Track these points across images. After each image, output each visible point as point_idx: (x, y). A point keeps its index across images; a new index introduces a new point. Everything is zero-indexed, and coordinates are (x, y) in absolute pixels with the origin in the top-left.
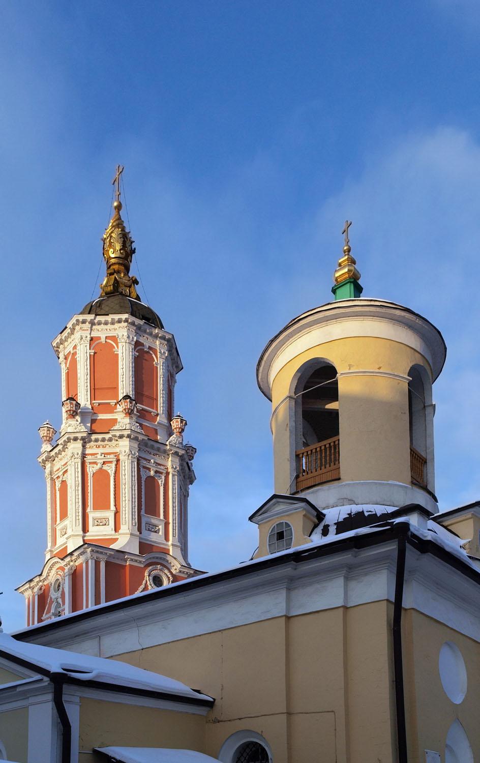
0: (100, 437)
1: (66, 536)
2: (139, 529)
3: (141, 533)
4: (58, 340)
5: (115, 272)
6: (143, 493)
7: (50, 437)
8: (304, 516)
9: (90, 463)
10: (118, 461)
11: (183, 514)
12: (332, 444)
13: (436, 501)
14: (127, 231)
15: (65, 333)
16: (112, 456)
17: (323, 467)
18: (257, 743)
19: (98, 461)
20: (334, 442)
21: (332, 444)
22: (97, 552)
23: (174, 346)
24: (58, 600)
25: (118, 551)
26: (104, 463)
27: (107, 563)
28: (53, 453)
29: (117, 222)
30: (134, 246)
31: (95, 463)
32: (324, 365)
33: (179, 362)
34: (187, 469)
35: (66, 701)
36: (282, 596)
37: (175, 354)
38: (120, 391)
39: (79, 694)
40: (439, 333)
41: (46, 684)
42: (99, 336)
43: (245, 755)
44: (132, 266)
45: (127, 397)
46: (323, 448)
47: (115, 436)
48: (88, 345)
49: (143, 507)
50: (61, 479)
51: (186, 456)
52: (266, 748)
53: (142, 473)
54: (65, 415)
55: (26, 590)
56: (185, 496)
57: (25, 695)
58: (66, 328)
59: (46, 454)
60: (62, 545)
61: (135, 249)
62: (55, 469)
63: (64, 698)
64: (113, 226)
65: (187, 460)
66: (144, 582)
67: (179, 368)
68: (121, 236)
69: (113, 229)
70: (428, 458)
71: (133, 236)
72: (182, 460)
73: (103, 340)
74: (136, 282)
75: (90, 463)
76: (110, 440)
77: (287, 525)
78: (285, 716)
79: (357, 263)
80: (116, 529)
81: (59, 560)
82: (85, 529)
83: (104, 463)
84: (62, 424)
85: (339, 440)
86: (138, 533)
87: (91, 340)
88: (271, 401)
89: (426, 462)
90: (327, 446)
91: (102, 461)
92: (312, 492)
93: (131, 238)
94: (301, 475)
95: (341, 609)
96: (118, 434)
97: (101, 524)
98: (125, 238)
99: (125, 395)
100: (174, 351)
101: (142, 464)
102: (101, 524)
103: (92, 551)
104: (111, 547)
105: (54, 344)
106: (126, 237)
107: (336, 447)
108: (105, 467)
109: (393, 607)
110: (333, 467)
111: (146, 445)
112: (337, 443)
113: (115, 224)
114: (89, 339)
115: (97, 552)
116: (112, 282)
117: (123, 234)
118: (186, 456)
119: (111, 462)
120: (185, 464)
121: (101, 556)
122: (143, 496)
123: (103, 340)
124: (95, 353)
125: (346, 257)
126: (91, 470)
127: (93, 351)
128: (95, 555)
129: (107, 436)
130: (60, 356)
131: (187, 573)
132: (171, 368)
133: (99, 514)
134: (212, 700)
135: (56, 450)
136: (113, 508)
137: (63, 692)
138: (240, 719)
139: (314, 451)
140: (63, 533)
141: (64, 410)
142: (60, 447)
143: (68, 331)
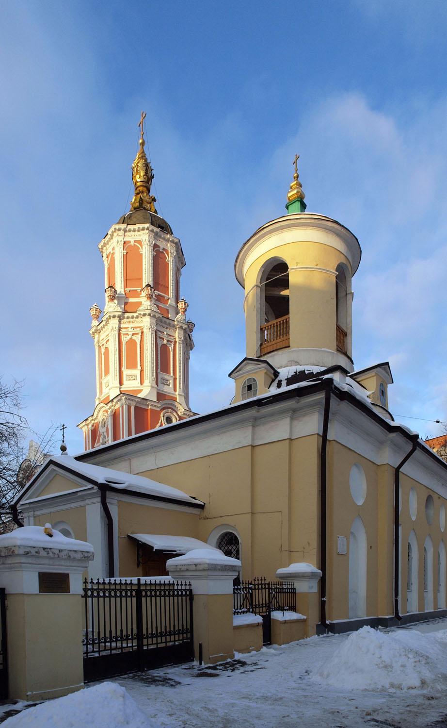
0: (130, 315)
1: (109, 388)
3: (158, 386)
4: (102, 244)
7: (97, 316)
9: (124, 334)
10: (142, 333)
12: (285, 321)
13: (353, 364)
14: (148, 161)
16: (138, 329)
17: (278, 338)
18: (232, 533)
19: (129, 333)
21: (285, 321)
23: (180, 248)
26: (133, 334)
27: (136, 408)
28: (99, 327)
30: (153, 172)
32: (279, 263)
39: (116, 498)
41: (96, 491)
42: (129, 240)
43: (224, 540)
44: (152, 188)
45: (148, 285)
46: (279, 323)
47: (140, 314)
48: (122, 247)
49: (159, 367)
50: (104, 346)
51: (188, 330)
52: (236, 534)
54: (107, 299)
56: (187, 359)
57: (83, 498)
58: (108, 234)
61: (154, 175)
63: (108, 501)
65: (188, 332)
66: (160, 421)
68: (144, 165)
71: (152, 165)
72: (185, 332)
73: (132, 243)
74: (154, 200)
75: (124, 334)
77: (254, 380)
80: (142, 383)
81: (105, 405)
82: (121, 383)
83: (133, 334)
85: (289, 318)
86: (156, 386)
89: (346, 335)
90: (282, 322)
91: (132, 333)
94: (264, 344)
95: (288, 441)
96: (142, 313)
97: (131, 379)
99: (147, 284)
102: (131, 379)
103: (126, 398)
105: (100, 247)
107: (287, 322)
108: (134, 338)
109: (321, 439)
110: (285, 337)
111: (161, 321)
112: (288, 320)
113: (140, 156)
114: (123, 242)
116: (138, 200)
118: (188, 330)
121: (131, 402)
123: (132, 243)
124: (127, 253)
125: (296, 182)
126: (125, 339)
127: (126, 252)
128: (128, 402)
129: (135, 315)
131: (189, 415)
134: (203, 504)
135: (101, 325)
136: (139, 367)
137: (107, 496)
139: (272, 326)
140: (107, 386)
141: (107, 295)
142: (104, 323)
143: (109, 236)
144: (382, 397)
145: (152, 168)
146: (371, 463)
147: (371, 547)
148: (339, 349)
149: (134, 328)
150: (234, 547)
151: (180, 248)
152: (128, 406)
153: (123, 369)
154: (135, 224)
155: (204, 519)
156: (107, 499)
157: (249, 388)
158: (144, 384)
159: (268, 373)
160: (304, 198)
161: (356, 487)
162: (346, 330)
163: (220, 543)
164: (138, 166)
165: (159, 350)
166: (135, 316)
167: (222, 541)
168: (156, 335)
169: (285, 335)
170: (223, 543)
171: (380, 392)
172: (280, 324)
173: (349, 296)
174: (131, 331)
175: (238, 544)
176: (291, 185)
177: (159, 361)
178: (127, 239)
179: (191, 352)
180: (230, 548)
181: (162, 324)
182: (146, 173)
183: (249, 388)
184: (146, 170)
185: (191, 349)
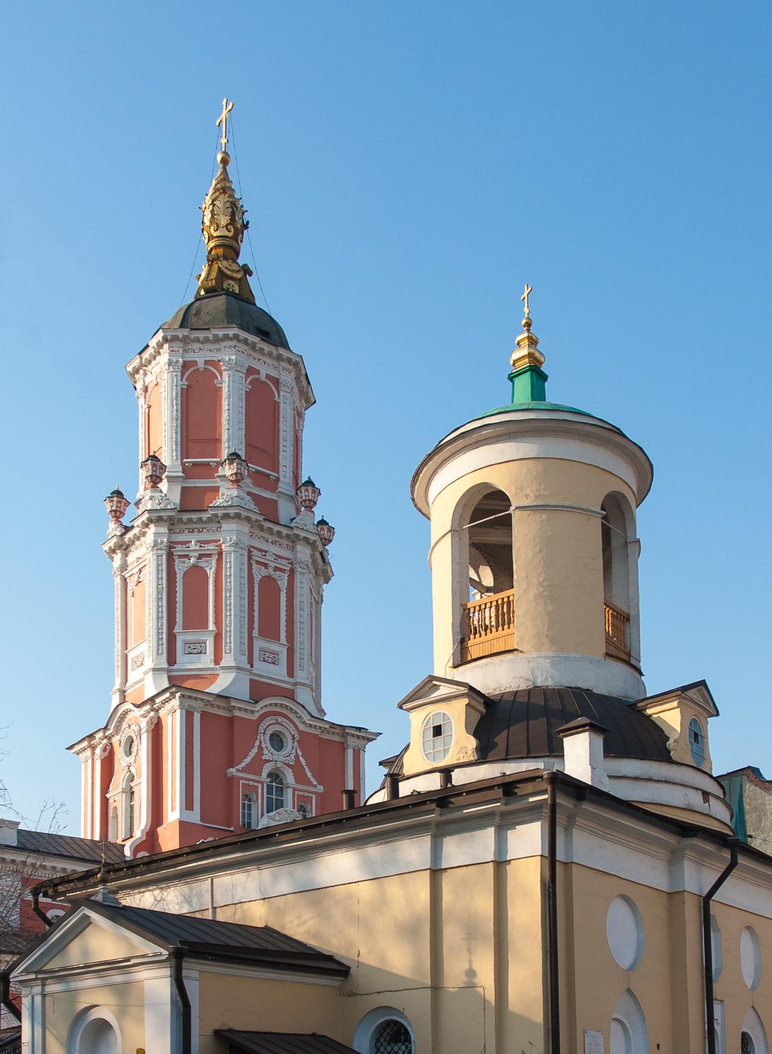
0: (194, 516)
2: (251, 661)
3: (252, 666)
4: (136, 363)
5: (217, 258)
6: (256, 603)
8: (467, 705)
9: (180, 556)
10: (220, 554)
11: (314, 645)
12: (506, 600)
13: (641, 674)
14: (237, 196)
15: (146, 355)
18: (398, 1022)
19: (191, 554)
20: (508, 597)
21: (506, 600)
22: (190, 697)
23: (304, 372)
24: (131, 769)
25: (218, 696)
26: (200, 557)
27: (204, 715)
29: (222, 184)
30: (247, 217)
31: (187, 557)
33: (310, 394)
34: (320, 561)
35: (188, 978)
36: (426, 841)
37: (304, 383)
38: (225, 445)
39: (199, 967)
40: (641, 449)
42: (195, 359)
43: (385, 1035)
44: (244, 248)
47: (216, 516)
48: (179, 374)
49: (256, 625)
52: (409, 1028)
53: (254, 571)
55: (84, 749)
56: (317, 603)
58: (147, 346)
59: (115, 540)
60: (136, 683)
61: (248, 223)
62: (136, 576)
63: (185, 973)
64: (216, 190)
66: (257, 743)
67: (309, 402)
68: (228, 205)
69: (217, 194)
70: (632, 613)
71: (245, 203)
72: (313, 550)
73: (201, 365)
75: (180, 556)
76: (210, 520)
78: (429, 991)
79: (540, 341)
80: (217, 659)
81: (132, 707)
83: (200, 557)
84: (138, 490)
86: (248, 667)
87: (183, 367)
88: (429, 519)
89: (628, 620)
91: (196, 554)
92: (480, 666)
93: (242, 206)
96: (220, 513)
97: (195, 651)
98: (235, 209)
100: (303, 378)
101: (254, 558)
102: (195, 651)
103: (182, 696)
104: (206, 691)
105: (130, 369)
106: (235, 205)
108: (202, 564)
109: (547, 862)
112: (511, 598)
113: (218, 186)
115: (190, 697)
116: (214, 275)
117: (231, 202)
119: (210, 555)
120: (318, 555)
121: (194, 703)
122: (256, 608)
123: (201, 365)
124: (189, 386)
125: (526, 335)
126: (181, 567)
127: (186, 383)
128: (187, 702)
129: (205, 516)
130: (137, 386)
131: (320, 728)
132: (298, 404)
133: (191, 636)
134: (389, 779)
136: (211, 626)
138: (379, 993)
140: (139, 663)
143: (150, 351)
144: (695, 745)
145: (245, 208)
146: (651, 890)
147: (658, 1046)
148: (613, 651)
149: (201, 542)
150: (403, 1048)
151: (304, 372)
152: (187, 711)
153: (178, 628)
154: (208, 329)
155: (349, 995)
156: (183, 971)
157: (437, 731)
158: (223, 664)
159: (475, 704)
160: (541, 363)
161: (619, 935)
162: (625, 609)
163: (378, 1040)
164: (214, 205)
165: (256, 589)
166: (204, 519)
167: (382, 1035)
168: (250, 557)
169: (506, 627)
170: (382, 1040)
171: (690, 737)
172: (503, 603)
173: (631, 548)
174: (194, 551)
175: (410, 1042)
176: (518, 338)
177: (256, 614)
178: (190, 357)
179: (325, 586)
180: (396, 1048)
181: (263, 534)
182: (233, 221)
183: (437, 731)
184: (233, 215)
185: (327, 581)
